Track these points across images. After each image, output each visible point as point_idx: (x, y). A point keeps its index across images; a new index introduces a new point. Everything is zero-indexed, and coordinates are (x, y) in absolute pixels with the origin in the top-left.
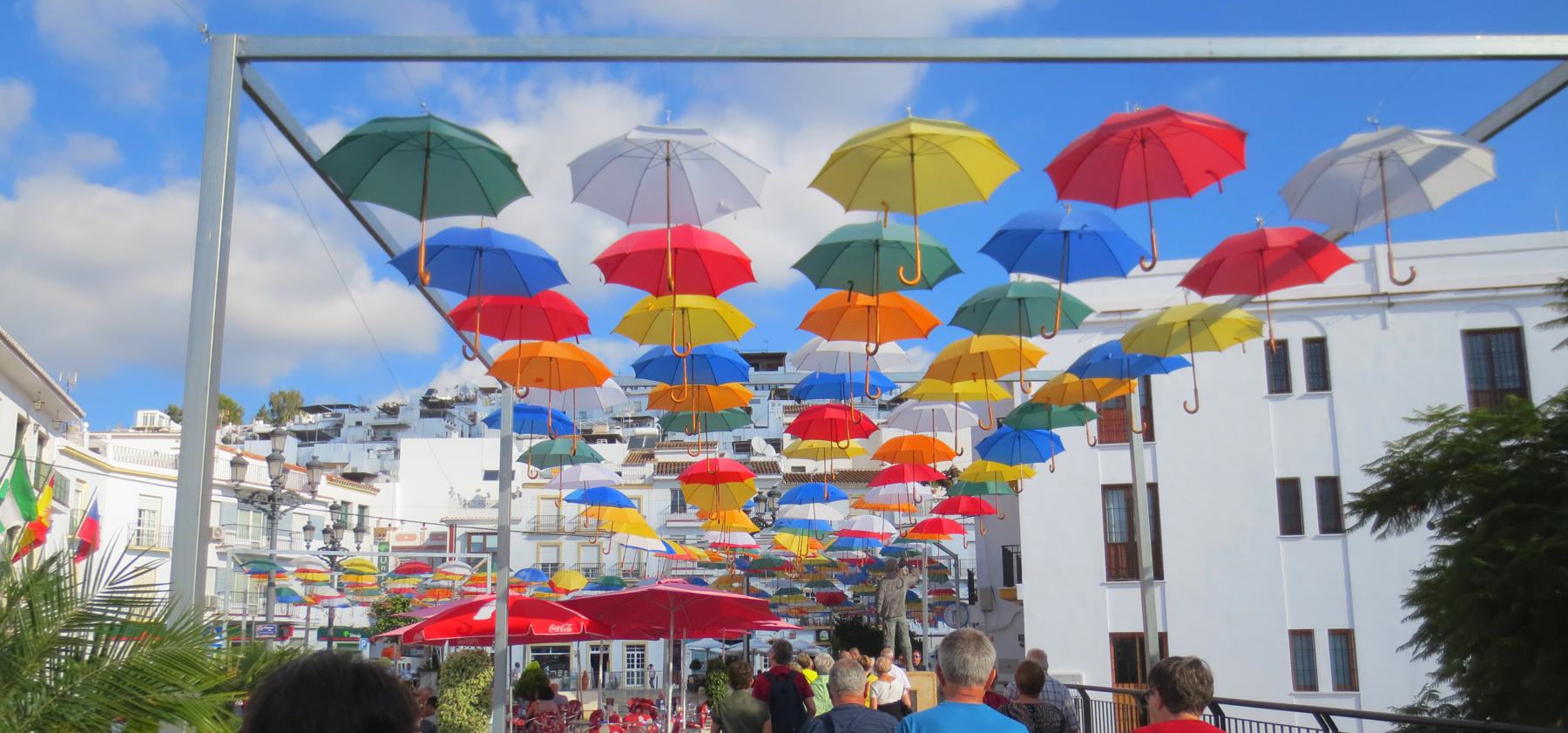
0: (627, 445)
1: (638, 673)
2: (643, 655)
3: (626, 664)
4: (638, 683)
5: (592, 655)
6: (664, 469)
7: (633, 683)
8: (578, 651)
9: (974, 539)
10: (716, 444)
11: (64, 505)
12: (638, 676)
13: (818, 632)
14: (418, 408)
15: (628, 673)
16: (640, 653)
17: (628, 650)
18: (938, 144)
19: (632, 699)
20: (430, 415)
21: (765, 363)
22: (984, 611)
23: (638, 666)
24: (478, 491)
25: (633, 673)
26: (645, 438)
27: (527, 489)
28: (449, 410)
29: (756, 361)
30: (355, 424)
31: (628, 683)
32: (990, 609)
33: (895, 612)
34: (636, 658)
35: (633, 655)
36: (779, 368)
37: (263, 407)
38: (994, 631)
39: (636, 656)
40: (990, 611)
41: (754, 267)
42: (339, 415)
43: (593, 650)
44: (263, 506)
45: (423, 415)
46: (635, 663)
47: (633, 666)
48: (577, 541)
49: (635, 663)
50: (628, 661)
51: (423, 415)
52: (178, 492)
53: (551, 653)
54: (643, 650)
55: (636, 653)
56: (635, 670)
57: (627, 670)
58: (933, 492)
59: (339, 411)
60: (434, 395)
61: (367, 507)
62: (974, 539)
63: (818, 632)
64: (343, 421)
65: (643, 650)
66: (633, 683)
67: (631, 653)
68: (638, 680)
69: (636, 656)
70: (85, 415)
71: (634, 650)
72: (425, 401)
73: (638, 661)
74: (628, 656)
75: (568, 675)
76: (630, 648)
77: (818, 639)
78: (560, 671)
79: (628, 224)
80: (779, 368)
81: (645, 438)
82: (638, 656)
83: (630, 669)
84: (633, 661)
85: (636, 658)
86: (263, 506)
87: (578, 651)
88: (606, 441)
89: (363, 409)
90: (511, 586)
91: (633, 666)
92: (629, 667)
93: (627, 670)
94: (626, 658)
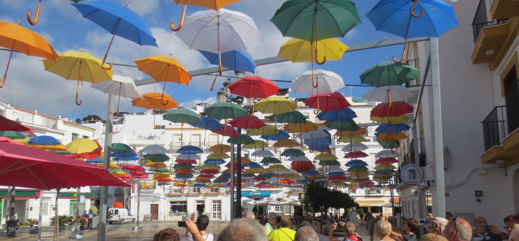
1: (218, 213)
2: (220, 205)
4: (218, 217)
7: (216, 217)
8: (56, 205)
9: (224, 120)
12: (218, 214)
13: (300, 195)
15: (213, 213)
16: (219, 204)
17: (213, 203)
18: (325, 7)
23: (218, 210)
24: (150, 134)
25: (216, 213)
27: (168, 131)
31: (213, 217)
34: (217, 207)
35: (216, 205)
36: (286, 94)
39: (217, 205)
41: (356, 113)
43: (198, 202)
46: (217, 209)
48: (172, 154)
49: (217, 209)
50: (213, 208)
52: (105, 144)
53: (179, 204)
55: (217, 204)
56: (217, 212)
57: (213, 212)
61: (79, 134)
62: (224, 120)
63: (300, 195)
65: (220, 203)
66: (216, 217)
67: (215, 204)
68: (218, 216)
69: (217, 205)
71: (216, 203)
73: (218, 208)
74: (214, 205)
75: (187, 214)
76: (214, 202)
77: (300, 198)
78: (183, 212)
79: (177, 3)
80: (286, 94)
82: (218, 205)
83: (214, 212)
84: (216, 208)
85: (217, 207)
87: (56, 205)
91: (216, 210)
92: (214, 210)
93: (213, 212)
94: (212, 207)
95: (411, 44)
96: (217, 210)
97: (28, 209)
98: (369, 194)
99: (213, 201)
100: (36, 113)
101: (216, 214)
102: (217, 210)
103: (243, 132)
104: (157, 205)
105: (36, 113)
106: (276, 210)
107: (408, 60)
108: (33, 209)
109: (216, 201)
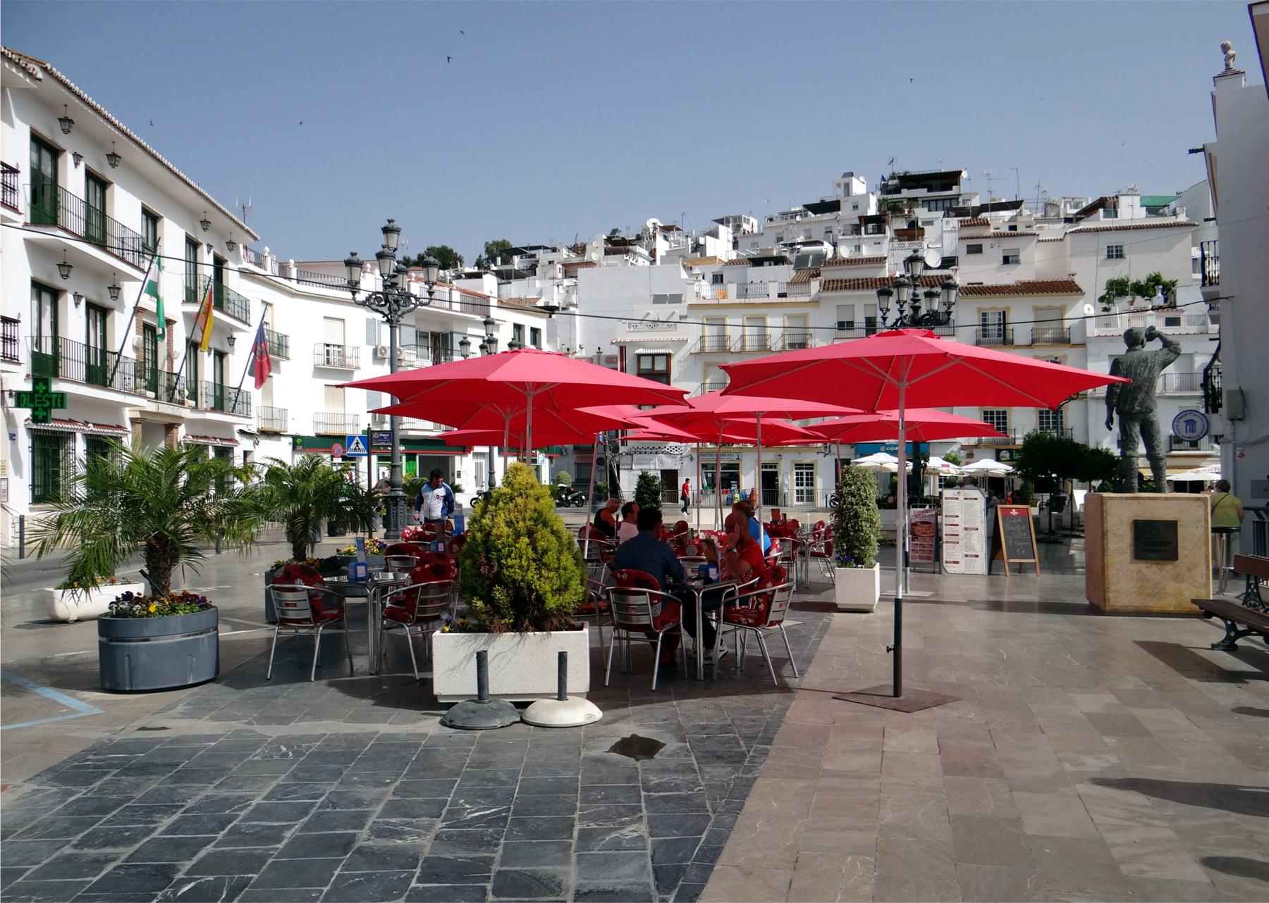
0: (792, 266)
2: (812, 474)
3: (795, 482)
5: (763, 472)
6: (831, 286)
10: (885, 258)
11: (245, 323)
14: (603, 246)
15: (798, 491)
17: (796, 469)
19: (879, 508)
20: (615, 253)
21: (938, 183)
22: (1231, 420)
25: (807, 485)
26: (811, 257)
28: (631, 247)
29: (928, 182)
30: (1210, 647)
31: (798, 500)
32: (1241, 417)
33: (1141, 405)
34: (805, 477)
35: (802, 474)
37: (480, 256)
38: (1244, 444)
39: (804, 474)
40: (1240, 420)
42: (534, 256)
44: (380, 309)
45: (607, 252)
46: (805, 482)
47: (802, 485)
49: (805, 482)
50: (797, 479)
51: (607, 252)
54: (813, 469)
58: (1132, 303)
59: (533, 252)
60: (617, 234)
64: (538, 261)
65: (813, 469)
69: (804, 474)
70: (259, 238)
71: (803, 469)
72: (609, 240)
81: (811, 257)
82: (807, 474)
83: (800, 488)
85: (805, 477)
86: (380, 309)
88: (773, 263)
89: (554, 250)
90: (517, 352)
95: (738, 347)
96: (805, 484)
97: (453, 475)
98: (1171, 450)
99: (796, 465)
100: (369, 270)
101: (802, 494)
102: (805, 484)
103: (427, 566)
104: (981, 245)
105: (369, 270)
106: (1004, 412)
107: (1086, 402)
108: (462, 474)
109: (802, 465)
